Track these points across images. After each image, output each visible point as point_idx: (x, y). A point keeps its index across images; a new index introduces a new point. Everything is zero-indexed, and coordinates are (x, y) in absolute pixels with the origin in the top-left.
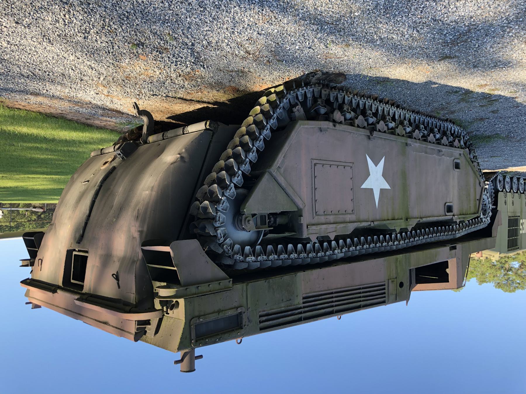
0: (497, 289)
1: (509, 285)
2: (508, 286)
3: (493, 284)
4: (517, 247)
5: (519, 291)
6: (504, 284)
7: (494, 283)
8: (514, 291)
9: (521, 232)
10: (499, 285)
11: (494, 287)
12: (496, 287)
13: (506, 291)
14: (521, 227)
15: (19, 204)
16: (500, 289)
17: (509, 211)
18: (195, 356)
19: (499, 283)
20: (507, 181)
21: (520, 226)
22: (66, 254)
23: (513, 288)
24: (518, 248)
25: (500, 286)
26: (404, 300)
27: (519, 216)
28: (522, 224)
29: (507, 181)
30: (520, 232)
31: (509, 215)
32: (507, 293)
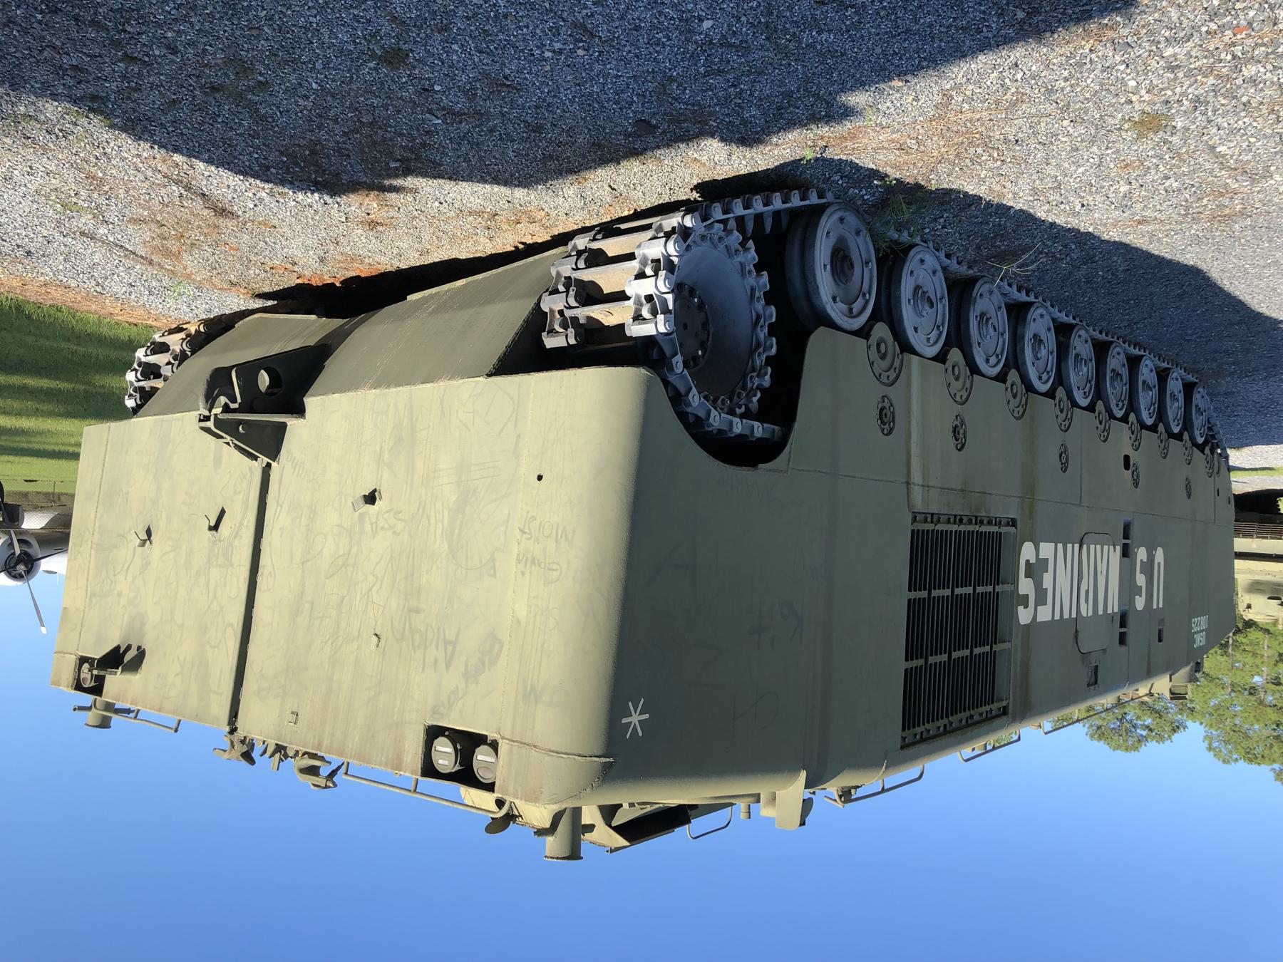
0: (1096, 742)
1: (1124, 734)
2: (1121, 735)
3: (1086, 729)
4: (995, 706)
5: (1151, 747)
6: (1114, 729)
7: (1087, 726)
8: (1136, 749)
9: (1024, 616)
10: (1099, 733)
11: (1088, 737)
12: (1092, 737)
13: (1118, 747)
14: (1025, 586)
15: (18, 540)
16: (1102, 742)
17: (916, 477)
18: (583, 823)
19: (1099, 727)
20: (1144, 382)
21: (1015, 582)
22: (249, 645)
23: (1135, 739)
24: (1004, 712)
25: (1103, 734)
26: (1231, 571)
27: (1013, 523)
28: (1035, 570)
29: (1144, 382)
30: (1014, 615)
31: (919, 506)
32: (1118, 752)
